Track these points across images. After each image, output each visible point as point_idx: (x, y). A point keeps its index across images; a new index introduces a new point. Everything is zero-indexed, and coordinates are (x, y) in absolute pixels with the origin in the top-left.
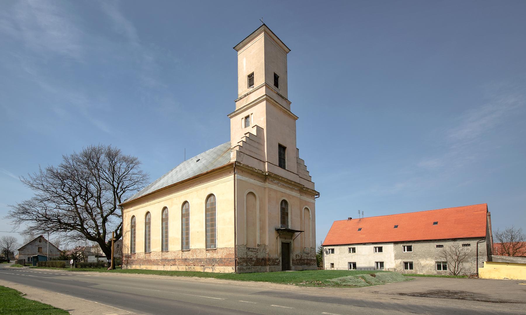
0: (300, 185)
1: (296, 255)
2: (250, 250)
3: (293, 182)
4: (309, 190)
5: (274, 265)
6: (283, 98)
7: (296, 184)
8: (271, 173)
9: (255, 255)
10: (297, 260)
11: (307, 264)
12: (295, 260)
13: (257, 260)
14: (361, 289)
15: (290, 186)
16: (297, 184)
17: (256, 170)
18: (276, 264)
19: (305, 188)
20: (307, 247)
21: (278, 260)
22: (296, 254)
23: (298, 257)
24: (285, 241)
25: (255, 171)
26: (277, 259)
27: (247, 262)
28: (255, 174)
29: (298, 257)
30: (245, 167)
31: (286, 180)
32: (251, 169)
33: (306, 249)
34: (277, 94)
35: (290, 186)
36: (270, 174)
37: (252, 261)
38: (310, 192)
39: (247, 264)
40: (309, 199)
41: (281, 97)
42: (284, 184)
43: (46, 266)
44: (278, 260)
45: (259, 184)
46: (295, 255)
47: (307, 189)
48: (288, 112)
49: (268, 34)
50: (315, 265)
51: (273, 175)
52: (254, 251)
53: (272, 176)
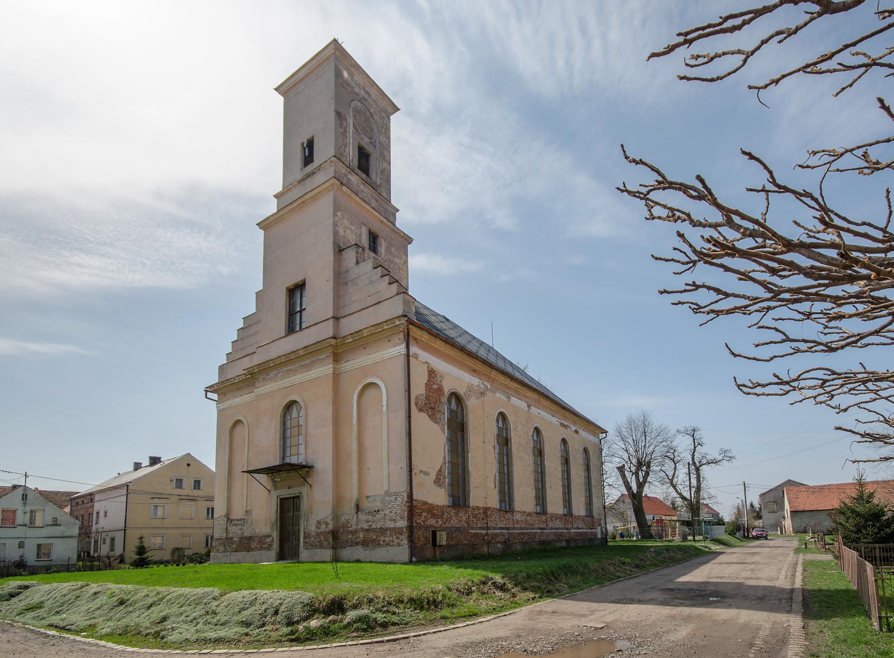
0: (321, 343)
1: (319, 522)
2: (233, 522)
3: (300, 351)
4: (365, 334)
5: (261, 548)
6: (315, 173)
7: (309, 348)
8: (250, 369)
9: (240, 532)
10: (318, 534)
11: (365, 543)
12: (314, 534)
13: (240, 541)
14: (55, 596)
15: (304, 363)
16: (312, 347)
17: (235, 380)
18: (264, 546)
19: (349, 337)
20: (375, 494)
21: (271, 539)
22: (317, 519)
23: (323, 526)
24: (285, 493)
25: (236, 381)
26: (269, 536)
27: (225, 545)
28: (241, 385)
29: (323, 526)
30: (221, 386)
31: (283, 357)
32: (229, 384)
33: (370, 499)
34: (300, 182)
35: (304, 363)
36: (250, 371)
37: (233, 543)
38: (373, 334)
39: (225, 549)
40: (378, 354)
41: (310, 176)
42: (290, 368)
43: (436, 561)
44: (271, 539)
45: (248, 399)
46: (315, 522)
47: (355, 335)
48: (306, 197)
49: (289, 89)
50: (399, 545)
51: (255, 368)
52: (240, 524)
53: (256, 371)
